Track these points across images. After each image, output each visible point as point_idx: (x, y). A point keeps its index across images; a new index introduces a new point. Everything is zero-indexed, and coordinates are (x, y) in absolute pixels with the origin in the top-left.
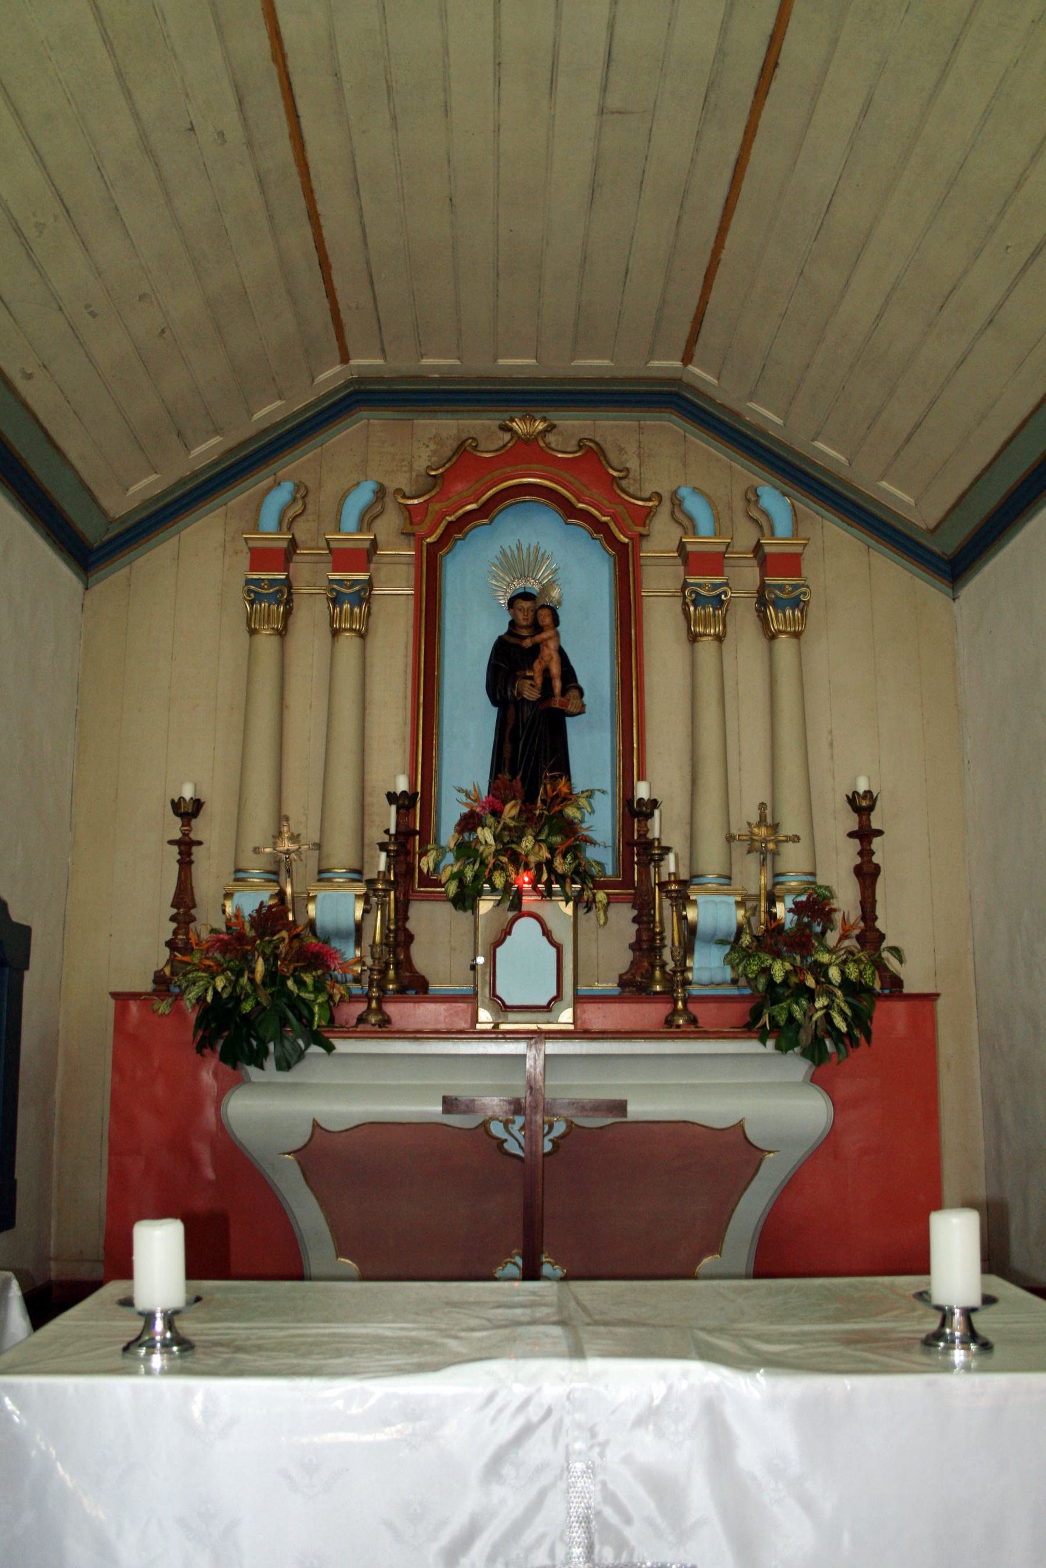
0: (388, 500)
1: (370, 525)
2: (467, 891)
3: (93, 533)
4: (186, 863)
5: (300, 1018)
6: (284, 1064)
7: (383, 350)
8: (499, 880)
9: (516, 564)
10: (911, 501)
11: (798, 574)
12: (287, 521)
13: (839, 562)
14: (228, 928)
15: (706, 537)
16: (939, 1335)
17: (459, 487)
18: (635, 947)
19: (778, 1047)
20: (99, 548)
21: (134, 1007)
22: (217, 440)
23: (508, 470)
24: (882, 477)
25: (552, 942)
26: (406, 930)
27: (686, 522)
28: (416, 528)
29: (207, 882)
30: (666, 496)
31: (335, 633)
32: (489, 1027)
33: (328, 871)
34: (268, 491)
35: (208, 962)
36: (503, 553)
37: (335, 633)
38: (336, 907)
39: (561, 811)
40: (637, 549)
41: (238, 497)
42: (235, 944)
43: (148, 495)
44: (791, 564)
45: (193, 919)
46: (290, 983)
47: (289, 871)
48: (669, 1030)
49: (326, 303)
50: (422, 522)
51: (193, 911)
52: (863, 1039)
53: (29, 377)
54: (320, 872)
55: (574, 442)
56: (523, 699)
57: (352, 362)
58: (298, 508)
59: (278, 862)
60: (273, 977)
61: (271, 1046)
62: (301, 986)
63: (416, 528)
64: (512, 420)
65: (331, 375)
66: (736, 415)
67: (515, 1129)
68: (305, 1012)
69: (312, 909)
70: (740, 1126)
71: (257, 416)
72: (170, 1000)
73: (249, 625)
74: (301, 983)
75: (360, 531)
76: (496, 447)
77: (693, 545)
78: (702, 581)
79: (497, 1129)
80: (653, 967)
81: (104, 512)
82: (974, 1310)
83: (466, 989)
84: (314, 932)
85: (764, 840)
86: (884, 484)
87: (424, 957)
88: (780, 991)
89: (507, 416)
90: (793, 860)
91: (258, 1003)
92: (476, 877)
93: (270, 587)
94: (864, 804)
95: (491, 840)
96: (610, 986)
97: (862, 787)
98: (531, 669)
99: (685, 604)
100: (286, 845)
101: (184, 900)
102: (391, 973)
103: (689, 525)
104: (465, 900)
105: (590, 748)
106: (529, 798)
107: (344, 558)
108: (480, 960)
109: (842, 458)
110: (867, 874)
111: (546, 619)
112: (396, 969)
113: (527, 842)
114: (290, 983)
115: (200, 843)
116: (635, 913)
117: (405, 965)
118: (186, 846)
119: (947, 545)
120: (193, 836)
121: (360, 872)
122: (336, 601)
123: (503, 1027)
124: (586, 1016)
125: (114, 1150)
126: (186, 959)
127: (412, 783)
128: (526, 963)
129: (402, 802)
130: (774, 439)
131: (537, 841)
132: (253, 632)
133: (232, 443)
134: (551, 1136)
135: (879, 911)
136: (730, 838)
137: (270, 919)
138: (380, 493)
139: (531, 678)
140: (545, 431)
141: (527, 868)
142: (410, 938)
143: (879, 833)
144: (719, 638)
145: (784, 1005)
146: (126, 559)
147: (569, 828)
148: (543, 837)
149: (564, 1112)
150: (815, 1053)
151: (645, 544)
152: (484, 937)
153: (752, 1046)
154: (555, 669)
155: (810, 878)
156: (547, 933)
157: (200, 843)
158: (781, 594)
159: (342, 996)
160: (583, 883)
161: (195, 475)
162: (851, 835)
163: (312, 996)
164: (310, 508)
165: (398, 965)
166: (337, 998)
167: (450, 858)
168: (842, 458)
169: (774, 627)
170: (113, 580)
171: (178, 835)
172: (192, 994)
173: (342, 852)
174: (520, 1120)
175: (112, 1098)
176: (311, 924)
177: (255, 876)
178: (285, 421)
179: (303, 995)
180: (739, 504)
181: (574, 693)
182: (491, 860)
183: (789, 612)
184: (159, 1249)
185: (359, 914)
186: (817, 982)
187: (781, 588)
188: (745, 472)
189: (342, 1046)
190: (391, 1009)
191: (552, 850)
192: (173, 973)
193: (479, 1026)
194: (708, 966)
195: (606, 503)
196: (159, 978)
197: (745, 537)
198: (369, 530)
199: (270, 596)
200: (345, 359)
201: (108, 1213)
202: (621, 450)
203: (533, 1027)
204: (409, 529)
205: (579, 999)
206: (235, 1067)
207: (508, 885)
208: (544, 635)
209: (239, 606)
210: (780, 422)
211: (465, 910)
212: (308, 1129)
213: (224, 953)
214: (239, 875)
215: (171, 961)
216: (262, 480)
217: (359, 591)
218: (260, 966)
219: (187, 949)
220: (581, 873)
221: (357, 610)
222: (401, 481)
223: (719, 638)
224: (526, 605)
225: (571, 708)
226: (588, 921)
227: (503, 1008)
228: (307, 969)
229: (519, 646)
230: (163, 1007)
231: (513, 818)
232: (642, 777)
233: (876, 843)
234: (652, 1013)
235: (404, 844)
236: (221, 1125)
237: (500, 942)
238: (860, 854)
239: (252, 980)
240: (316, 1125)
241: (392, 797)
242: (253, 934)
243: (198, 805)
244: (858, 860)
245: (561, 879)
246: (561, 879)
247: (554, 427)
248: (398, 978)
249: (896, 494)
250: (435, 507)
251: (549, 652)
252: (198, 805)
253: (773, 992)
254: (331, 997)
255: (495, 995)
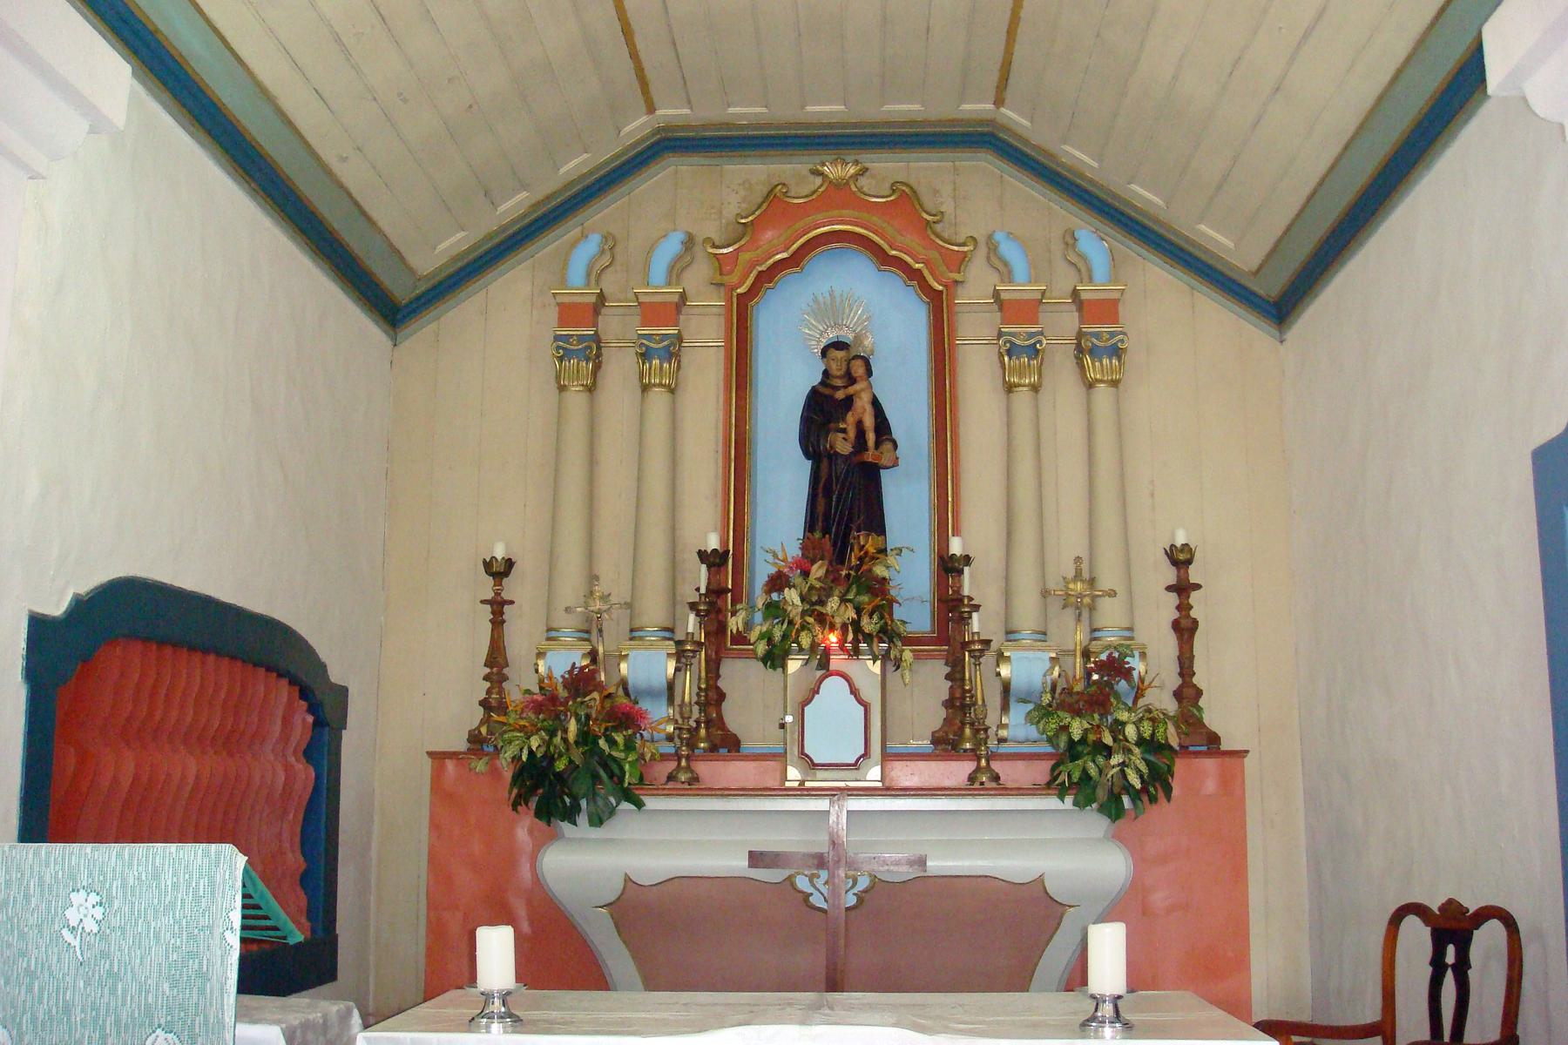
0: (698, 249)
1: (678, 276)
2: (776, 651)
3: (402, 292)
4: (498, 622)
5: (611, 776)
6: (596, 820)
7: (689, 102)
8: (805, 640)
9: (830, 310)
10: (1231, 245)
11: (1115, 321)
12: (594, 274)
13: (1160, 303)
14: (541, 688)
15: (1022, 286)
16: (1093, 1018)
17: (769, 234)
18: (948, 704)
19: (1075, 803)
20: (407, 306)
21: (450, 765)
22: (524, 194)
23: (819, 216)
24: (1200, 221)
25: (860, 701)
26: (718, 688)
27: (1001, 268)
28: (726, 279)
29: (521, 636)
30: (982, 240)
31: (645, 388)
32: (796, 784)
33: (640, 629)
34: (574, 244)
35: (522, 723)
36: (815, 300)
37: (645, 388)
38: (647, 666)
39: (870, 570)
40: (951, 296)
41: (547, 247)
42: (548, 705)
43: (455, 252)
44: (1107, 310)
45: (506, 678)
46: (602, 742)
47: (600, 631)
48: (973, 786)
49: (630, 63)
50: (732, 272)
51: (505, 671)
52: (1161, 794)
53: (344, 160)
54: (632, 630)
55: (888, 185)
56: (837, 454)
57: (658, 112)
58: (606, 260)
59: (589, 620)
60: (586, 737)
61: (583, 803)
62: (612, 746)
63: (726, 279)
64: (823, 164)
65: (637, 127)
66: (1051, 156)
67: (819, 883)
68: (616, 771)
69: (623, 666)
70: (1040, 880)
71: (563, 170)
72: (485, 759)
73: (558, 378)
74: (612, 743)
75: (669, 284)
76: (806, 192)
77: (1009, 291)
78: (1020, 332)
79: (802, 883)
80: (963, 724)
81: (411, 271)
82: (1119, 997)
83: (779, 749)
84: (627, 693)
85: (1080, 594)
86: (1202, 227)
87: (735, 717)
88: (1080, 748)
89: (817, 159)
90: (1111, 615)
91: (571, 762)
92: (785, 637)
93: (580, 342)
94: (1182, 557)
95: (797, 601)
96: (925, 744)
97: (1180, 540)
98: (844, 420)
99: (1001, 355)
100: (598, 605)
101: (496, 659)
102: (703, 732)
103: (1006, 273)
104: (775, 658)
105: (905, 498)
106: (840, 557)
107: (653, 312)
108: (789, 719)
109: (1160, 202)
110: (1185, 629)
111: (858, 369)
112: (707, 728)
113: (833, 604)
114: (602, 742)
115: (512, 602)
116: (948, 669)
117: (715, 722)
118: (498, 606)
119: (1271, 287)
120: (505, 596)
121: (671, 630)
122: (645, 356)
123: (808, 784)
124: (893, 774)
125: (432, 906)
126: (502, 719)
127: (724, 542)
128: (834, 723)
129: (713, 560)
130: (1091, 181)
131: (843, 600)
132: (562, 388)
133: (540, 196)
134: (855, 890)
135: (1198, 666)
136: (1045, 593)
137: (580, 682)
138: (689, 243)
139: (844, 431)
140: (856, 177)
141: (832, 628)
142: (722, 696)
143: (1197, 587)
144: (1035, 388)
145: (1079, 762)
146: (434, 313)
147: (879, 588)
148: (850, 597)
149: (867, 867)
150: (1112, 809)
151: (960, 290)
152: (793, 696)
153: (1052, 803)
154: (869, 422)
155: (1127, 634)
156: (854, 692)
157: (512, 602)
158: (1100, 345)
159: (653, 755)
160: (891, 641)
161: (504, 228)
162: (1169, 588)
163: (622, 755)
164: (618, 257)
165: (708, 723)
166: (648, 757)
167: (758, 617)
168: (1160, 202)
169: (1091, 374)
170: (423, 334)
171: (490, 595)
172: (509, 753)
173: (654, 612)
174: (824, 874)
175: (430, 853)
176: (624, 684)
177: (567, 635)
178: (591, 173)
179: (614, 754)
180: (1057, 247)
181: (888, 446)
182: (798, 620)
183: (1106, 361)
184: (496, 951)
185: (671, 671)
186: (1115, 740)
187: (1098, 335)
188: (1065, 214)
189: (651, 803)
190: (702, 768)
191: (859, 611)
192: (490, 732)
193: (788, 784)
194: (1017, 726)
195: (920, 249)
196: (475, 739)
197: (1065, 280)
198: (678, 284)
199: (579, 347)
200: (651, 109)
201: (427, 964)
202: (936, 192)
203: (842, 784)
204: (718, 279)
205: (887, 757)
206: (549, 823)
207: (814, 646)
208: (857, 387)
209: (547, 348)
210: (1095, 165)
211: (774, 667)
212: (619, 885)
213: (537, 713)
214: (551, 634)
215: (486, 720)
216: (567, 232)
217: (669, 346)
218: (573, 727)
219: (502, 708)
220: (887, 633)
221: (666, 365)
222: (711, 230)
223: (1035, 388)
224: (840, 354)
225: (884, 462)
226: (894, 677)
227: (811, 765)
228: (617, 729)
229: (831, 398)
230: (480, 766)
231: (819, 579)
232: (956, 532)
233: (1194, 597)
234: (957, 771)
235: (713, 606)
236: (537, 881)
237: (808, 701)
238: (1178, 608)
239: (565, 740)
240: (628, 879)
241: (703, 556)
242: (566, 694)
243: (509, 564)
244: (1176, 615)
245: (868, 638)
246: (868, 638)
247: (865, 170)
248: (709, 737)
249: (1215, 238)
250: (745, 257)
251: (863, 405)
252: (509, 564)
253: (1073, 751)
254: (642, 756)
255: (803, 753)
